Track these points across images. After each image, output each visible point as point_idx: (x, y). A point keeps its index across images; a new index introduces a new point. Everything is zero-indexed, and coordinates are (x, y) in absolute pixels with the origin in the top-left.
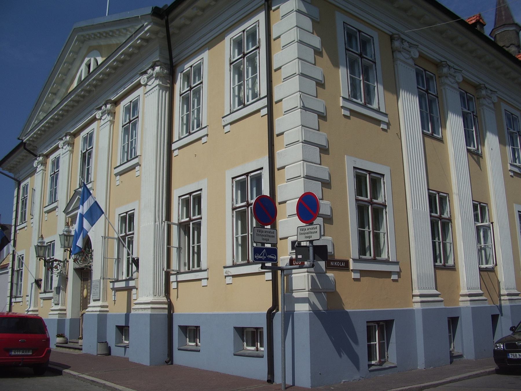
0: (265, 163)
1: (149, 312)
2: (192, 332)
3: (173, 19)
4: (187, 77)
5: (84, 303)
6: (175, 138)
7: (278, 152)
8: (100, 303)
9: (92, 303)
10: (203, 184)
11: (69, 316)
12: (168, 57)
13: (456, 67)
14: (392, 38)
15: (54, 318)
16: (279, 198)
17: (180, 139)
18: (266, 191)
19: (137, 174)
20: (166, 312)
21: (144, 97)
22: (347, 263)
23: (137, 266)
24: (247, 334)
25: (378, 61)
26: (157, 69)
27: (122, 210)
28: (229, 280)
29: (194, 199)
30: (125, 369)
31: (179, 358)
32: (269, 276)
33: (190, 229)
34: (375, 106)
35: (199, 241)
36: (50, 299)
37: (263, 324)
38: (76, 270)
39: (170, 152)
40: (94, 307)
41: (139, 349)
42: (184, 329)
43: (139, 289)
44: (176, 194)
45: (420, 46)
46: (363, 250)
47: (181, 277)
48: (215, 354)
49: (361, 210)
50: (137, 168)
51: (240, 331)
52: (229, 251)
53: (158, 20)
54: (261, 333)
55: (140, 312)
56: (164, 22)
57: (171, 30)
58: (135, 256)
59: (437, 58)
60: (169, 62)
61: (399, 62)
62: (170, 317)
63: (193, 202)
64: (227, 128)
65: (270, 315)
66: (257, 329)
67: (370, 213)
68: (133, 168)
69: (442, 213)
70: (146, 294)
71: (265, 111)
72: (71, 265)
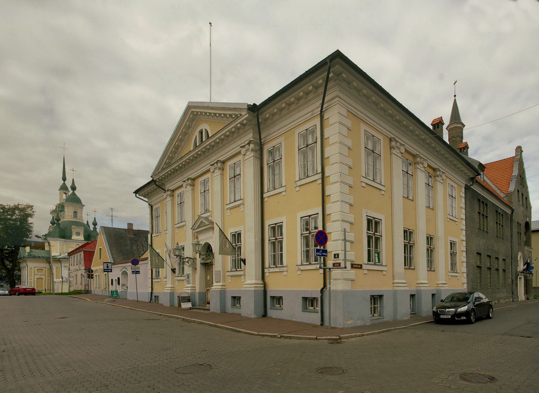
0: (320, 211)
1: (253, 289)
2: (278, 300)
3: (261, 114)
4: (271, 152)
5: (209, 283)
6: (266, 190)
7: (328, 206)
8: (221, 284)
9: (215, 284)
10: (282, 219)
11: (198, 290)
12: (259, 138)
13: (425, 158)
14: (391, 140)
15: (251, 289)
16: (327, 231)
17: (268, 192)
18: (320, 228)
19: (242, 210)
20: (263, 289)
21: (243, 163)
22: (361, 265)
23: (245, 264)
24: (309, 302)
25: (382, 155)
26: (252, 146)
27: (233, 230)
28: (299, 272)
29: (278, 226)
30: (239, 319)
31: (271, 313)
32: (322, 271)
33: (277, 245)
34: (378, 181)
35: (281, 250)
36: (183, 280)
37: (318, 295)
38: (201, 264)
39: (262, 199)
40: (216, 286)
41: (249, 308)
42: (273, 298)
43: (246, 276)
44: (267, 223)
45: (406, 145)
46: (369, 260)
47: (271, 270)
48: (291, 310)
49: (369, 238)
50: (242, 206)
51: (305, 299)
52: (299, 257)
53: (252, 113)
54: (317, 300)
55: (248, 289)
56: (256, 114)
57: (260, 120)
58: (242, 257)
59: (415, 152)
60: (259, 142)
61: (393, 155)
62: (265, 292)
63: (277, 229)
64: (298, 189)
65: (322, 291)
66: (314, 298)
67: (374, 241)
68: (239, 206)
69: (410, 240)
70: (250, 280)
71: (320, 181)
72: (199, 261)
